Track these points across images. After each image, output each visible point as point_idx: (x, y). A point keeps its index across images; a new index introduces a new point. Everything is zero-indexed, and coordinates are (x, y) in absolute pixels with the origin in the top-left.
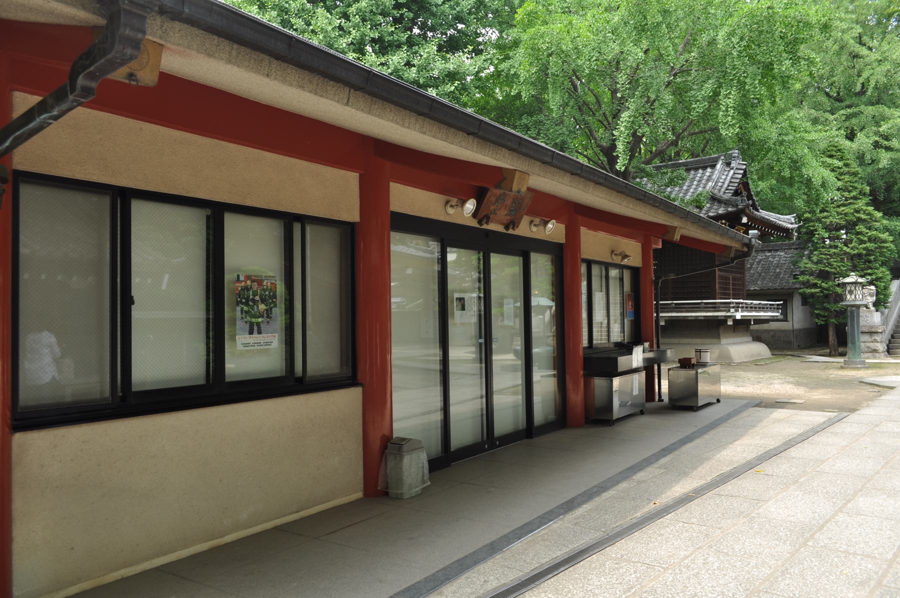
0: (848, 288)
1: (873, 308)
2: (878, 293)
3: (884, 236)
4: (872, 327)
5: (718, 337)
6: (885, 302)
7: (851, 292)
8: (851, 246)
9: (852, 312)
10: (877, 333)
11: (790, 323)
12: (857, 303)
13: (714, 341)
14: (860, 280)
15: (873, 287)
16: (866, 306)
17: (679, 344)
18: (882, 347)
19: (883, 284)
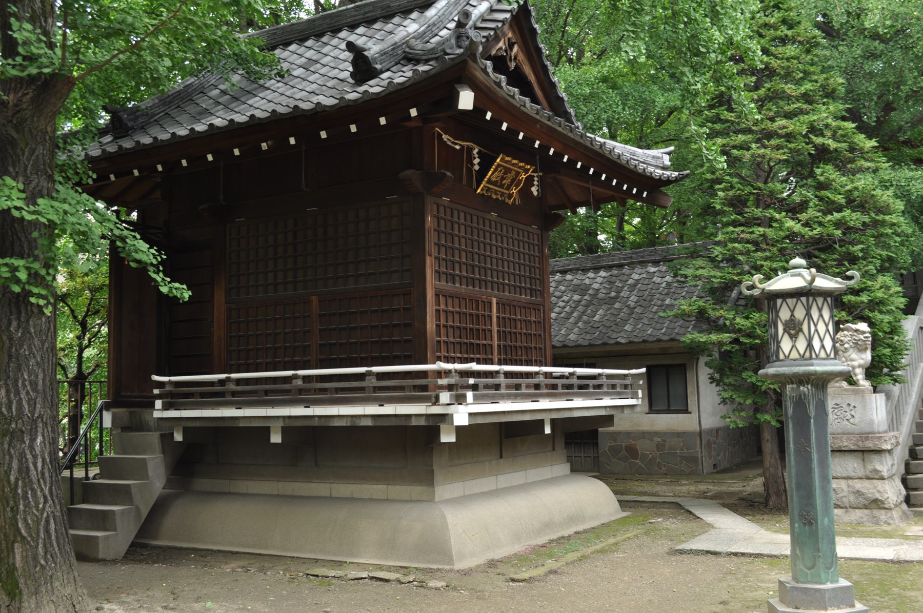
0: (784, 314)
1: (865, 384)
2: (876, 343)
3: (885, 196)
4: (866, 435)
5: (428, 480)
7: (793, 328)
8: (803, 216)
9: (800, 402)
10: (879, 452)
11: (694, 416)
12: (819, 367)
13: (416, 490)
14: (824, 282)
15: (863, 326)
16: (849, 378)
17: (352, 500)
18: (893, 491)
19: (887, 318)
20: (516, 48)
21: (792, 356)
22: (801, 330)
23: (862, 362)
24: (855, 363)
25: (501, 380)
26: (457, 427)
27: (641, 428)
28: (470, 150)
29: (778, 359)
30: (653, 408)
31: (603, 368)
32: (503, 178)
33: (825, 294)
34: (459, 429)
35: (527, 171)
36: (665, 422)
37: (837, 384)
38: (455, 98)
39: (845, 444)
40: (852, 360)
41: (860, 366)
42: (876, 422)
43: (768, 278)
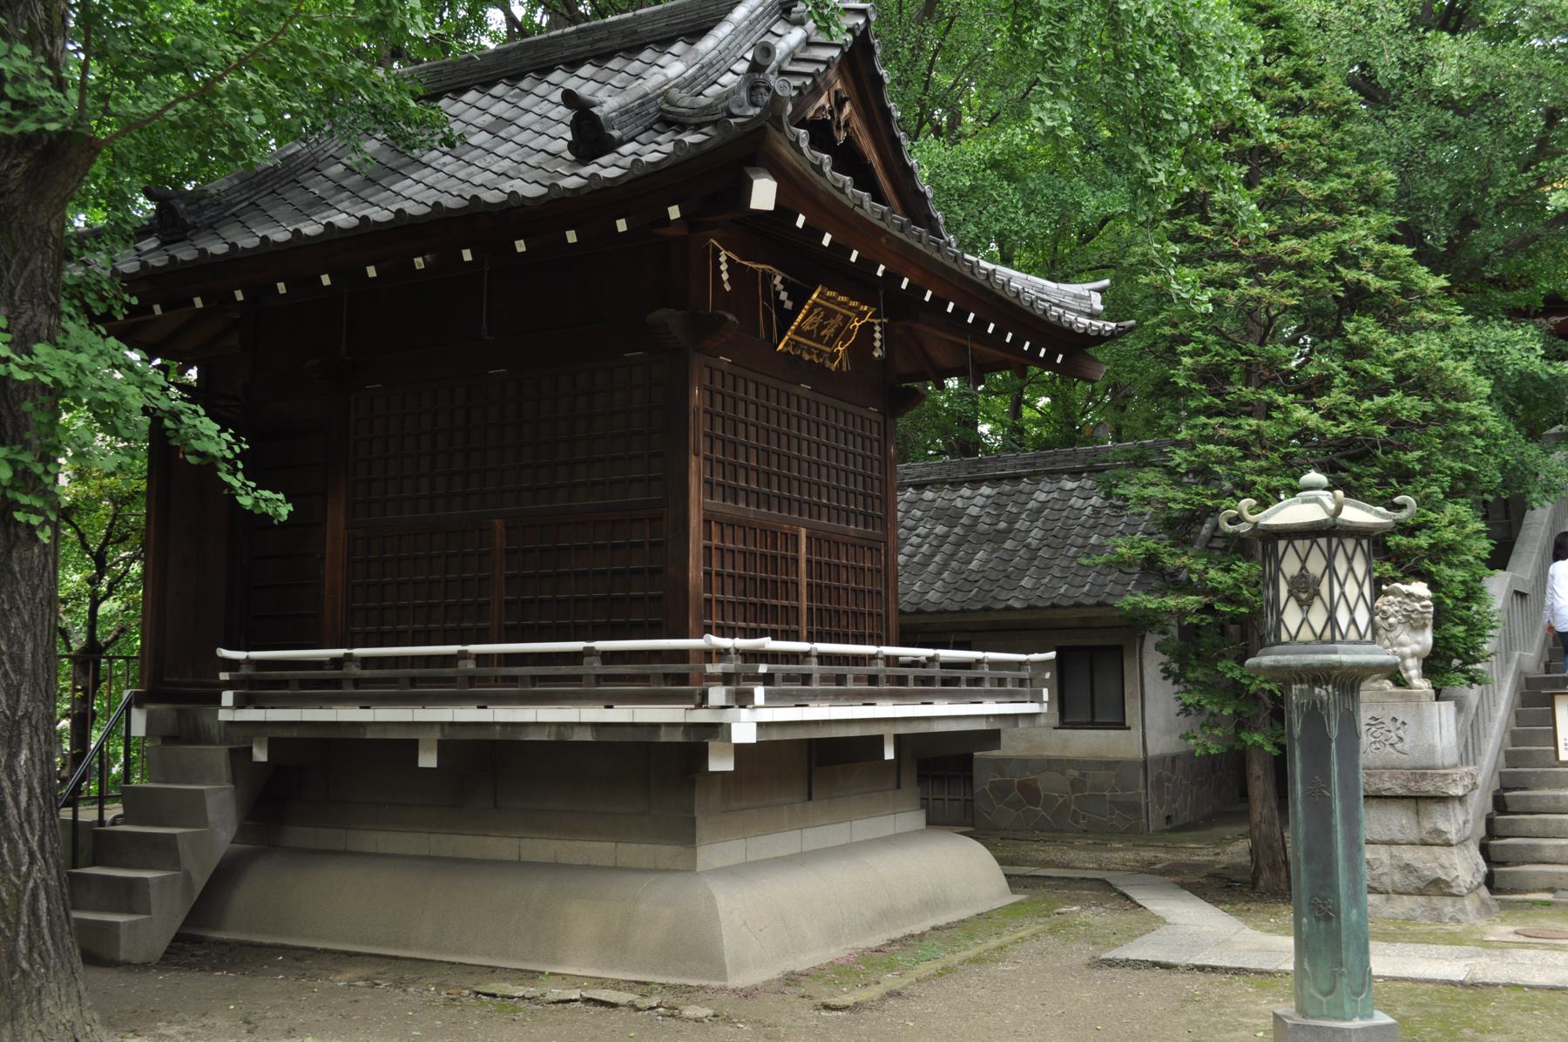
0: (1291, 566)
1: (1422, 685)
2: (1441, 617)
3: (1461, 371)
4: (1422, 771)
5: (684, 834)
6: (1470, 656)
7: (1305, 590)
8: (1324, 402)
9: (1315, 714)
10: (1443, 799)
11: (1136, 733)
12: (1346, 656)
13: (665, 852)
14: (1356, 514)
15: (1420, 588)
16: (1395, 674)
18: (1465, 866)
19: (1460, 575)
20: (847, 108)
21: (1301, 637)
22: (1317, 593)
23: (1417, 648)
24: (1407, 650)
25: (813, 666)
26: (737, 746)
28: (768, 278)
29: (1279, 642)
31: (984, 650)
32: (821, 327)
33: (1357, 533)
34: (741, 750)
35: (862, 315)
37: (1376, 685)
39: (1388, 785)
40: (1401, 645)
41: (1413, 655)
42: (1439, 748)
43: (1264, 504)
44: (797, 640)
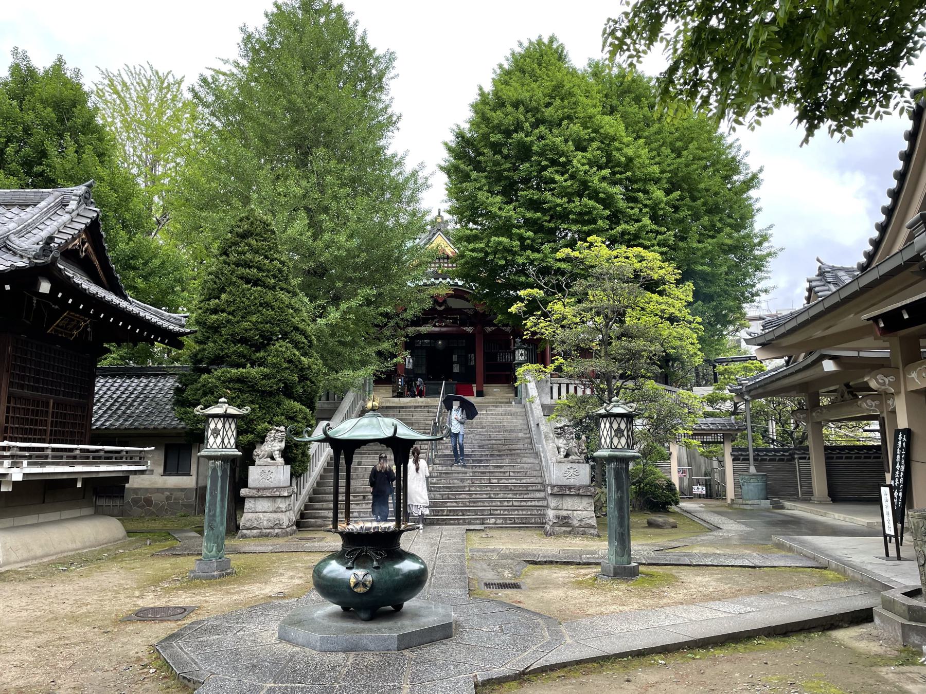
0: (212, 426)
1: (280, 460)
7: (216, 432)
20: (87, 245)
25: (49, 452)
26: (14, 482)
27: (156, 486)
30: (167, 472)
32: (67, 324)
33: (233, 416)
34: (15, 484)
35: (85, 321)
36: (174, 481)
38: (37, 285)
43: (206, 407)
44: (44, 443)
